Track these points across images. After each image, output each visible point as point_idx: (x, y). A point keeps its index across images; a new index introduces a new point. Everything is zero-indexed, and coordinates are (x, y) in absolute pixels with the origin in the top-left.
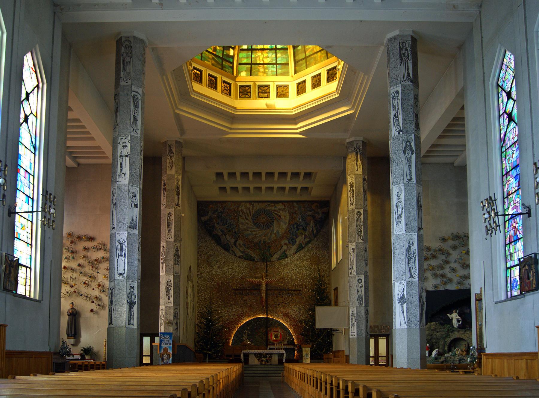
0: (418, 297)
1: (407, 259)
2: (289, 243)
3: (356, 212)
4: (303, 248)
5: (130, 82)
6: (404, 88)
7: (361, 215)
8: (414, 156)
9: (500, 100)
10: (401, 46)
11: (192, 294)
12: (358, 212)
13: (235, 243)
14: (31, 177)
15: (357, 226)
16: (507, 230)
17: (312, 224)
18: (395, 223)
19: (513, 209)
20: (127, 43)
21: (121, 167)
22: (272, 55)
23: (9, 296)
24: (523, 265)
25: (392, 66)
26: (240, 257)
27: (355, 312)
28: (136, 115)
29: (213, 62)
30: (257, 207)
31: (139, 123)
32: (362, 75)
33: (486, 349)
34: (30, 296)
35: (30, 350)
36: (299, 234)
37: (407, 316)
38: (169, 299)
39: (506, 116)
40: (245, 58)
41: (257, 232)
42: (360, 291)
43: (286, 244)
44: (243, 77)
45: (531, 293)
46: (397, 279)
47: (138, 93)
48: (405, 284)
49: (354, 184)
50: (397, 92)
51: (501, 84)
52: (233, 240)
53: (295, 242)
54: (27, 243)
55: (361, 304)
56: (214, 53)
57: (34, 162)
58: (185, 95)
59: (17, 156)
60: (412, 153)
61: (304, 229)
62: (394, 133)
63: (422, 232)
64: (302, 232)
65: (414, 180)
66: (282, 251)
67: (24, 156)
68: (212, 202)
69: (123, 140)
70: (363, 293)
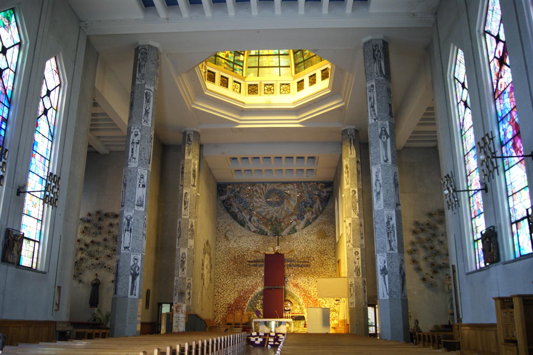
0: (398, 269)
1: (386, 233)
2: (298, 219)
3: (351, 191)
4: (310, 223)
5: (143, 82)
6: (378, 82)
7: (355, 193)
8: (389, 140)
9: (457, 90)
10: (374, 48)
11: (209, 266)
12: (353, 191)
13: (250, 220)
14: (47, 162)
15: (353, 203)
16: (472, 205)
17: (318, 202)
18: (375, 199)
19: (475, 186)
20: (143, 50)
21: (132, 152)
22: (276, 59)
23: (12, 269)
24: (484, 238)
25: (368, 65)
26: (254, 232)
27: (353, 282)
28: (147, 109)
29: (226, 66)
30: (270, 187)
31: (150, 115)
32: (347, 73)
33: (463, 320)
34: (36, 268)
35: (31, 319)
36: (306, 211)
37: (389, 286)
38: (183, 271)
39: (462, 103)
40: (253, 62)
41: (270, 209)
42: (357, 263)
43: (295, 220)
44: (252, 78)
45: (494, 264)
46: (379, 252)
47: (150, 90)
48: (386, 256)
49: (349, 166)
50: (372, 86)
51: (456, 77)
52: (248, 217)
53: (304, 218)
54: (38, 219)
55: (359, 275)
56: (226, 58)
57: (51, 149)
58: (200, 93)
59: (33, 143)
60: (387, 138)
61: (311, 207)
62: (371, 121)
63: (399, 208)
64: (310, 209)
65: (390, 161)
66: (292, 226)
67: (41, 143)
68: (229, 184)
69: (135, 130)
70: (360, 265)
